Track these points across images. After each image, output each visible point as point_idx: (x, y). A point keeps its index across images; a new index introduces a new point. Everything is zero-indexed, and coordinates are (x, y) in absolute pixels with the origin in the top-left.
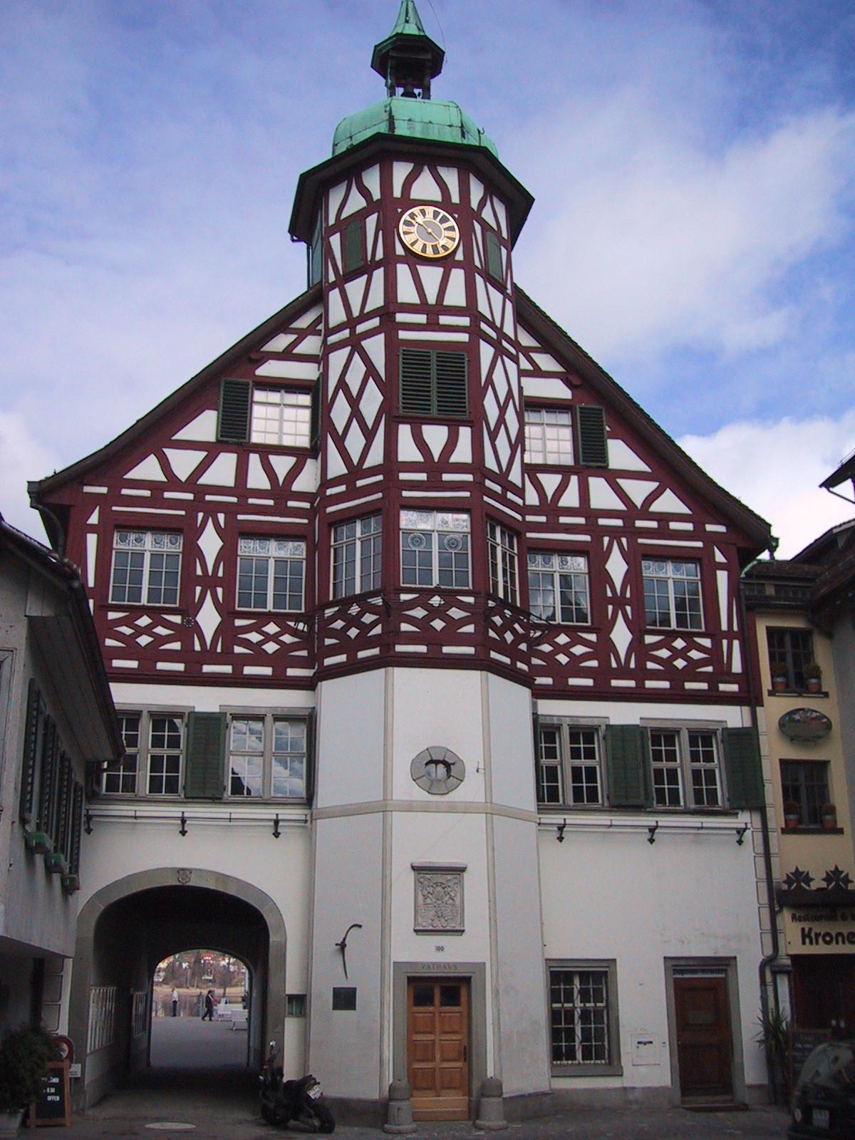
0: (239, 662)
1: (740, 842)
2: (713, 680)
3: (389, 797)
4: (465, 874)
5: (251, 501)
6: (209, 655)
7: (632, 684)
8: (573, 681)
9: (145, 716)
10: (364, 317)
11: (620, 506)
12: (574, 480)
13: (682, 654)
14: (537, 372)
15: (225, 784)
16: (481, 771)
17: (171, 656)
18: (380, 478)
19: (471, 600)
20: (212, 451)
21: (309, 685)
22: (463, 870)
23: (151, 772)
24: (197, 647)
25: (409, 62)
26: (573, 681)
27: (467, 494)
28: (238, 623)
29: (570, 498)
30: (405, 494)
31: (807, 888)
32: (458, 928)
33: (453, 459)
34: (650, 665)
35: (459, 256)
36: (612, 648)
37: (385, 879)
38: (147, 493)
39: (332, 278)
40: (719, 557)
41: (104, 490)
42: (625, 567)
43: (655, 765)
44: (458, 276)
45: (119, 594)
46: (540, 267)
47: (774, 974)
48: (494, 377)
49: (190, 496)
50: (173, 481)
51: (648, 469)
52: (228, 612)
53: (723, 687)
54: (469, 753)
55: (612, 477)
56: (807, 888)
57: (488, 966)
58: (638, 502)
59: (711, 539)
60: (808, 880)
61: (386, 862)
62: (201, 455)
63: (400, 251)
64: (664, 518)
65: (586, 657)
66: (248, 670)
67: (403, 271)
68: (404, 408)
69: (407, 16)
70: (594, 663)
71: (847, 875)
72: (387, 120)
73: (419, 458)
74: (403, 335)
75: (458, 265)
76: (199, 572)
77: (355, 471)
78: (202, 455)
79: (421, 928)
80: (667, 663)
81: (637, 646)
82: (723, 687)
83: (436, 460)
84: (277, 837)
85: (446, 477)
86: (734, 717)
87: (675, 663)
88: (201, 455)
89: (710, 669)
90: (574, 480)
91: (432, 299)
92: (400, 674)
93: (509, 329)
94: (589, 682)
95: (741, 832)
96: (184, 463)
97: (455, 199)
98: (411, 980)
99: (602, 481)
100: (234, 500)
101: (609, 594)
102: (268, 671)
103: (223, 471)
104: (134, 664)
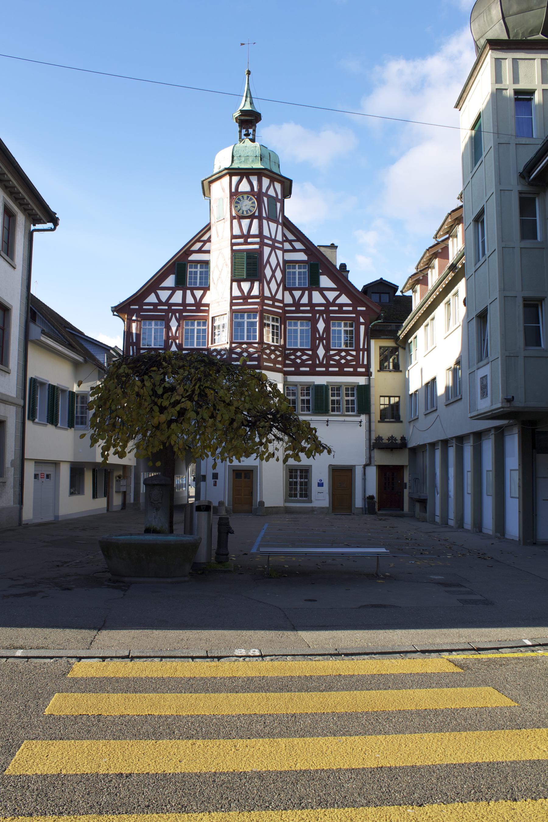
1: (360, 426)
5: (188, 308)
7: (324, 369)
8: (302, 369)
11: (324, 302)
12: (307, 292)
13: (344, 358)
14: (294, 250)
20: (173, 290)
25: (249, 121)
26: (302, 369)
29: (305, 300)
34: (332, 362)
38: (152, 307)
40: (362, 320)
41: (137, 307)
43: (332, 398)
44: (256, 222)
46: (293, 209)
49: (166, 307)
50: (161, 303)
51: (336, 287)
52: (327, 349)
53: (359, 370)
55: (321, 291)
58: (331, 300)
60: (396, 440)
62: (170, 292)
64: (341, 305)
65: (307, 360)
70: (310, 362)
72: (57, 517)
75: (256, 217)
78: (170, 292)
80: (338, 361)
82: (359, 370)
86: (362, 381)
88: (170, 292)
89: (354, 363)
90: (307, 292)
94: (308, 369)
95: (361, 422)
96: (164, 295)
97: (256, 189)
100: (182, 308)
101: (318, 336)
103: (177, 298)
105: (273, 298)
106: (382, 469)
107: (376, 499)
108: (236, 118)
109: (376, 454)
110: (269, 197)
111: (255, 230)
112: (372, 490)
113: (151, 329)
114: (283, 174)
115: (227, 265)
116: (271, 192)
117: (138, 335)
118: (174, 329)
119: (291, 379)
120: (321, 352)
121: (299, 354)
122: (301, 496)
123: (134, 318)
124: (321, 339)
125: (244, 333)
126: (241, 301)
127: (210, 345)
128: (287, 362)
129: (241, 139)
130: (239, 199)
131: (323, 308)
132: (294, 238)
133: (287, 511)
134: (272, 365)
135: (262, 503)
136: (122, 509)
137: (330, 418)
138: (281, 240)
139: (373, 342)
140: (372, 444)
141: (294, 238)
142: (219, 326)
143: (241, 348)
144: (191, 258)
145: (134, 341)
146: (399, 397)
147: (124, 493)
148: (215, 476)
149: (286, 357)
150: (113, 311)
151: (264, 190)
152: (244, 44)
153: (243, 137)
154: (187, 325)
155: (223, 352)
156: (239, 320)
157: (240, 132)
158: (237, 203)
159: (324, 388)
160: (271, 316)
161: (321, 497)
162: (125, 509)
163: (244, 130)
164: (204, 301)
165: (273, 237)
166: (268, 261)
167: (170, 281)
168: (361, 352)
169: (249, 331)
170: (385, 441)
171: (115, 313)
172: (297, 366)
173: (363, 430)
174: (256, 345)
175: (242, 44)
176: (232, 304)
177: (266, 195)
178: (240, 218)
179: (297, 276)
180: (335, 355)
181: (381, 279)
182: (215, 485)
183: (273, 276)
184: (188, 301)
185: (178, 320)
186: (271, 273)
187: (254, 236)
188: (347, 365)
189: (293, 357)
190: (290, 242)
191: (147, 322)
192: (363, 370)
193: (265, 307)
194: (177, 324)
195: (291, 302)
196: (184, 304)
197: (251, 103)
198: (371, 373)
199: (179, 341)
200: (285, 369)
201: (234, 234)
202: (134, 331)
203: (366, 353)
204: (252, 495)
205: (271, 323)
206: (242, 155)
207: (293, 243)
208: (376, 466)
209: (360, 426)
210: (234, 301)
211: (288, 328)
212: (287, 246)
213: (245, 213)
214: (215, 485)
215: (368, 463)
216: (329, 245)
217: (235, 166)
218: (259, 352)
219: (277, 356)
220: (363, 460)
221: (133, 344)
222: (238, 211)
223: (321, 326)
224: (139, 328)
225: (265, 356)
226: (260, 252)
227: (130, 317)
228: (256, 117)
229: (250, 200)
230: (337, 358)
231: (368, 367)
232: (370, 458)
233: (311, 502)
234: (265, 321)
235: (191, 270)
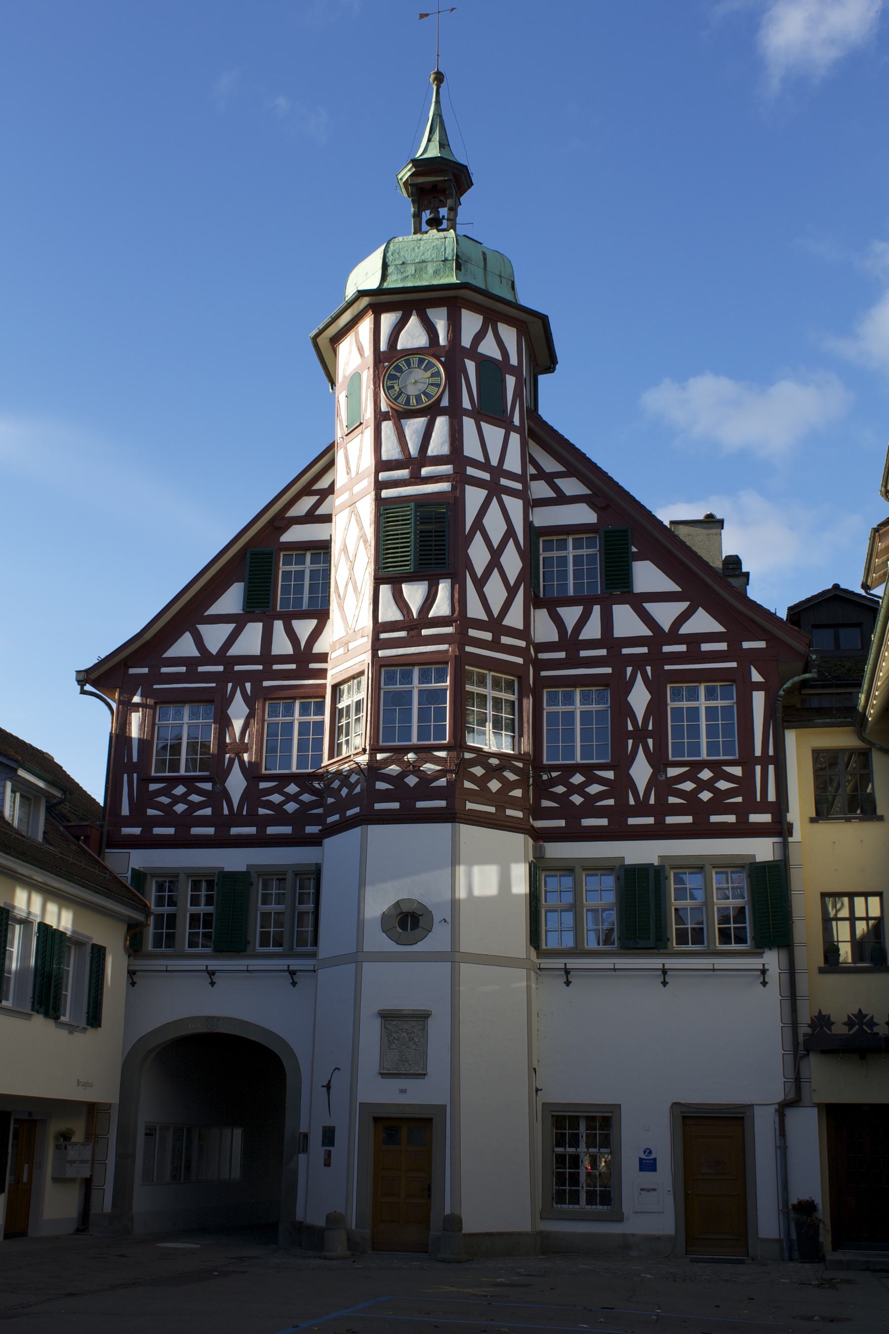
0: (263, 823)
1: (764, 983)
4: (431, 1022)
5: (275, 667)
6: (237, 819)
7: (650, 820)
8: (587, 822)
9: (182, 878)
11: (646, 632)
12: (597, 609)
13: (708, 785)
14: (561, 499)
15: (669, 936)
17: (204, 822)
20: (239, 622)
21: (315, 841)
23: (190, 929)
24: (226, 811)
25: (438, 188)
26: (587, 822)
28: (263, 785)
29: (592, 630)
31: (828, 1032)
32: (421, 1072)
34: (672, 800)
35: (445, 402)
38: (183, 669)
40: (756, 677)
41: (145, 670)
42: (648, 697)
44: (441, 423)
45: (553, 754)
48: (486, 521)
49: (220, 668)
50: (206, 657)
51: (677, 588)
52: (658, 762)
53: (754, 818)
55: (638, 602)
56: (828, 1032)
58: (666, 626)
59: (749, 659)
60: (872, 1024)
62: (230, 627)
65: (601, 796)
66: (271, 830)
70: (611, 802)
71: (872, 1017)
75: (443, 412)
78: (649, 606)
79: (386, 1072)
82: (754, 818)
84: (568, 985)
86: (762, 849)
87: (700, 796)
88: (230, 627)
89: (739, 799)
90: (597, 609)
92: (375, 831)
94: (604, 822)
96: (214, 636)
98: (376, 1120)
99: (627, 607)
100: (260, 667)
101: (630, 728)
103: (250, 641)
104: (171, 831)
105: (495, 624)
106: (836, 1116)
107: (823, 1212)
108: (406, 183)
109: (817, 1069)
110: (483, 362)
111: (439, 444)
112: (810, 1181)
114: (524, 300)
115: (366, 541)
116: (489, 348)
117: (145, 744)
118: (238, 725)
119: (557, 850)
120: (641, 771)
121: (578, 779)
122: (589, 1202)
123: (137, 699)
124: (640, 735)
125: (410, 721)
126: (403, 634)
127: (326, 762)
128: (546, 803)
130: (398, 369)
131: (645, 650)
132: (561, 468)
133: (547, 1246)
134: (492, 809)
135: (454, 1222)
136: (78, 1231)
137: (671, 963)
138: (518, 470)
139: (791, 737)
140: (801, 1039)
141: (561, 468)
142: (348, 707)
143: (399, 762)
144: (286, 537)
145: (135, 759)
146: (879, 894)
147: (88, 1184)
148: (329, 1136)
149: (543, 790)
150: (81, 682)
151: (466, 341)
152: (427, 15)
153: (425, 227)
154: (274, 713)
155: (354, 778)
156: (398, 687)
157: (417, 216)
158: (392, 377)
159: (652, 873)
160: (490, 675)
161: (650, 1206)
162: (83, 1230)
163: (428, 212)
164: (318, 648)
165: (494, 462)
166: (478, 524)
167: (231, 600)
168: (758, 768)
169: (423, 715)
170: (839, 1029)
171: (88, 688)
172: (565, 809)
173: (769, 1001)
174: (442, 754)
175: (422, 16)
176: (377, 644)
177: (473, 353)
178: (400, 415)
179: (571, 568)
180: (681, 779)
181: (836, 586)
182: (327, 1164)
184: (276, 650)
185: (249, 701)
186: (503, 560)
187: (438, 460)
188: (719, 804)
189: (560, 789)
190: (549, 478)
191: (172, 710)
192: (766, 818)
193: (468, 649)
194: (247, 711)
195: (555, 637)
196: (266, 656)
197: (443, 145)
198: (790, 826)
199: (250, 756)
200: (539, 824)
201: (384, 457)
202: (135, 733)
203: (771, 768)
204: (429, 1196)
205: (489, 692)
206: (409, 259)
207: (558, 481)
208: (819, 1106)
209: (764, 983)
210: (383, 636)
211: (547, 709)
212: (540, 490)
213: (413, 401)
214: (327, 1164)
215: (792, 1096)
216: (701, 517)
217: (389, 284)
218: (451, 772)
219: (508, 786)
220: (776, 1090)
221: (131, 768)
222: (396, 399)
223: (639, 698)
224: (150, 725)
225: (468, 785)
226: (456, 501)
227: (125, 698)
228: (454, 175)
229: (426, 370)
230: (688, 786)
231: (780, 808)
232: (798, 1081)
233: (619, 1218)
234: (469, 688)
235: (288, 568)
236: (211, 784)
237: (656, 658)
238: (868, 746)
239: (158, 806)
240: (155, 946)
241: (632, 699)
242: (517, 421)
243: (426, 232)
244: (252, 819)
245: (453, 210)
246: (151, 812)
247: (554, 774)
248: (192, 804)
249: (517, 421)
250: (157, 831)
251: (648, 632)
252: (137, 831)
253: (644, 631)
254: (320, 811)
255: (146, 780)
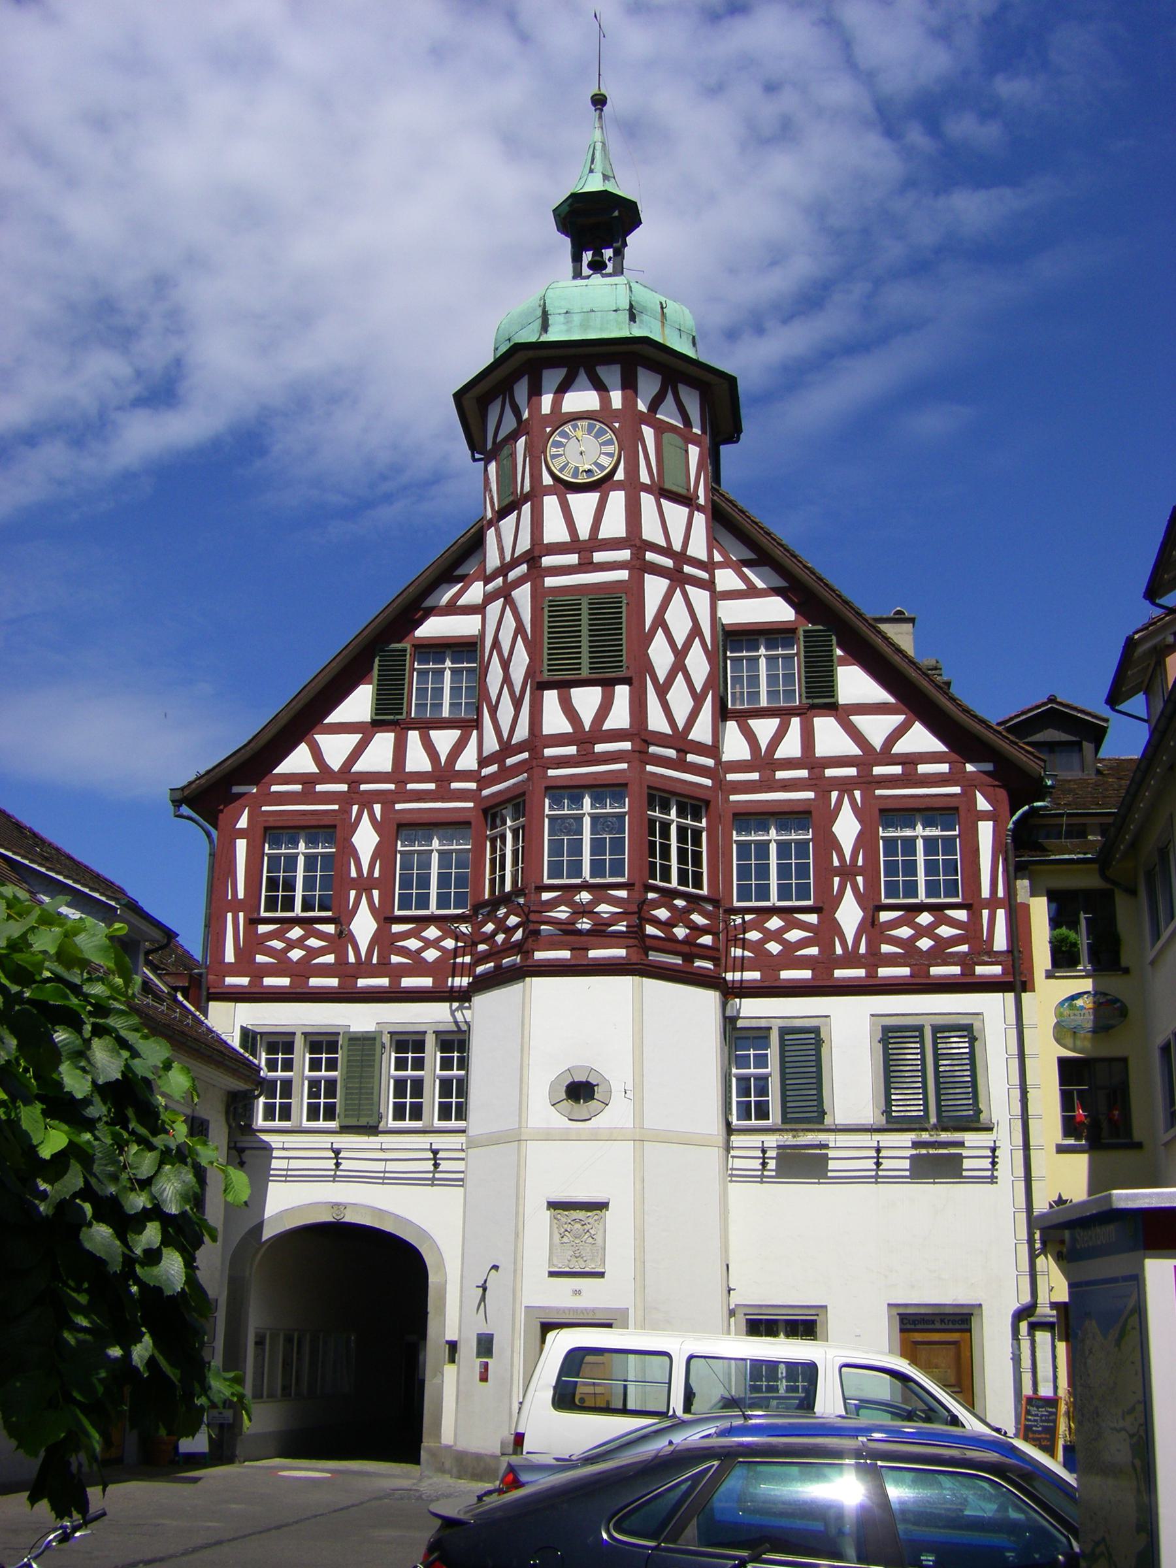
0: (397, 973)
2: (967, 962)
3: (524, 1125)
4: (608, 1214)
5: (410, 786)
6: (364, 968)
7: (861, 972)
8: (785, 974)
10: (515, 563)
11: (855, 750)
12: (795, 722)
13: (928, 931)
14: (751, 592)
16: (630, 1094)
17: (324, 971)
18: (526, 755)
19: (623, 894)
21: (463, 996)
22: (602, 1206)
26: (785, 974)
27: (625, 766)
29: (791, 747)
30: (551, 772)
33: (608, 725)
34: (886, 948)
35: (620, 475)
36: (838, 931)
37: (518, 1215)
39: (489, 515)
40: (982, 804)
42: (857, 827)
44: (617, 498)
47: (1033, 1327)
48: (668, 616)
49: (344, 787)
50: (326, 773)
51: (891, 699)
54: (616, 1074)
55: (843, 714)
57: (631, 1311)
58: (877, 742)
61: (519, 1196)
63: (547, 480)
64: (910, 761)
65: (804, 943)
67: (551, 503)
68: (549, 671)
69: (592, 162)
70: (814, 951)
73: (567, 728)
74: (550, 582)
75: (619, 486)
76: (354, 874)
77: (507, 748)
78: (855, 719)
80: (908, 945)
81: (870, 926)
83: (587, 729)
85: (599, 748)
88: (357, 737)
89: (964, 948)
90: (795, 722)
91: (584, 533)
92: (537, 984)
93: (698, 548)
94: (806, 974)
100: (392, 787)
101: (836, 863)
102: (427, 982)
103: (379, 755)
104: (285, 981)
111: (614, 525)
113: (296, 856)
119: (751, 1009)
129: (577, 275)
143: (570, 903)
145: (241, 895)
148: (485, 1345)
150: (177, 803)
153: (586, 271)
157: (577, 259)
166: (660, 621)
171: (185, 810)
181: (1052, 699)
182: (484, 1378)
183: (679, 666)
186: (689, 661)
187: (613, 544)
188: (940, 953)
196: (399, 773)
214: (484, 1378)
226: (635, 589)
236: (333, 926)
237: (867, 782)
238: (1108, 886)
239: (270, 952)
240: (265, 1119)
241: (837, 829)
242: (702, 501)
243: (588, 277)
244: (384, 968)
245: (619, 253)
246: (260, 958)
247: (748, 917)
248: (309, 949)
249: (702, 501)
250: (268, 981)
251: (857, 751)
252: (244, 981)
253: (851, 749)
254: (467, 959)
255: (254, 921)
